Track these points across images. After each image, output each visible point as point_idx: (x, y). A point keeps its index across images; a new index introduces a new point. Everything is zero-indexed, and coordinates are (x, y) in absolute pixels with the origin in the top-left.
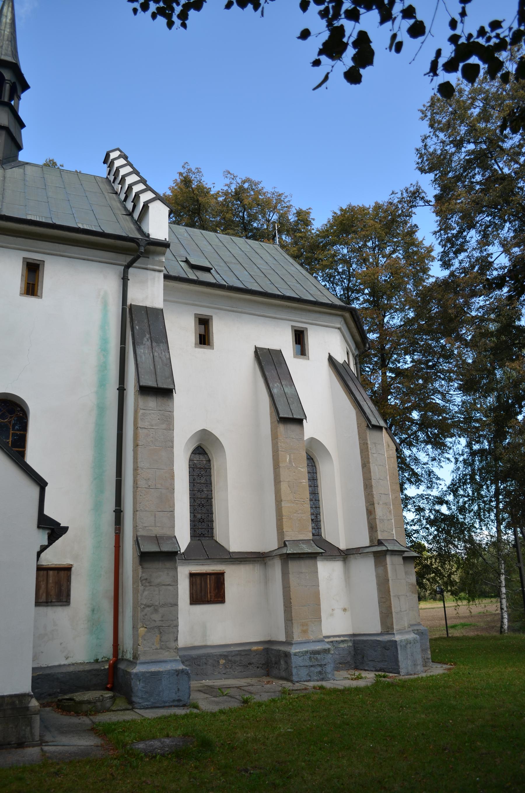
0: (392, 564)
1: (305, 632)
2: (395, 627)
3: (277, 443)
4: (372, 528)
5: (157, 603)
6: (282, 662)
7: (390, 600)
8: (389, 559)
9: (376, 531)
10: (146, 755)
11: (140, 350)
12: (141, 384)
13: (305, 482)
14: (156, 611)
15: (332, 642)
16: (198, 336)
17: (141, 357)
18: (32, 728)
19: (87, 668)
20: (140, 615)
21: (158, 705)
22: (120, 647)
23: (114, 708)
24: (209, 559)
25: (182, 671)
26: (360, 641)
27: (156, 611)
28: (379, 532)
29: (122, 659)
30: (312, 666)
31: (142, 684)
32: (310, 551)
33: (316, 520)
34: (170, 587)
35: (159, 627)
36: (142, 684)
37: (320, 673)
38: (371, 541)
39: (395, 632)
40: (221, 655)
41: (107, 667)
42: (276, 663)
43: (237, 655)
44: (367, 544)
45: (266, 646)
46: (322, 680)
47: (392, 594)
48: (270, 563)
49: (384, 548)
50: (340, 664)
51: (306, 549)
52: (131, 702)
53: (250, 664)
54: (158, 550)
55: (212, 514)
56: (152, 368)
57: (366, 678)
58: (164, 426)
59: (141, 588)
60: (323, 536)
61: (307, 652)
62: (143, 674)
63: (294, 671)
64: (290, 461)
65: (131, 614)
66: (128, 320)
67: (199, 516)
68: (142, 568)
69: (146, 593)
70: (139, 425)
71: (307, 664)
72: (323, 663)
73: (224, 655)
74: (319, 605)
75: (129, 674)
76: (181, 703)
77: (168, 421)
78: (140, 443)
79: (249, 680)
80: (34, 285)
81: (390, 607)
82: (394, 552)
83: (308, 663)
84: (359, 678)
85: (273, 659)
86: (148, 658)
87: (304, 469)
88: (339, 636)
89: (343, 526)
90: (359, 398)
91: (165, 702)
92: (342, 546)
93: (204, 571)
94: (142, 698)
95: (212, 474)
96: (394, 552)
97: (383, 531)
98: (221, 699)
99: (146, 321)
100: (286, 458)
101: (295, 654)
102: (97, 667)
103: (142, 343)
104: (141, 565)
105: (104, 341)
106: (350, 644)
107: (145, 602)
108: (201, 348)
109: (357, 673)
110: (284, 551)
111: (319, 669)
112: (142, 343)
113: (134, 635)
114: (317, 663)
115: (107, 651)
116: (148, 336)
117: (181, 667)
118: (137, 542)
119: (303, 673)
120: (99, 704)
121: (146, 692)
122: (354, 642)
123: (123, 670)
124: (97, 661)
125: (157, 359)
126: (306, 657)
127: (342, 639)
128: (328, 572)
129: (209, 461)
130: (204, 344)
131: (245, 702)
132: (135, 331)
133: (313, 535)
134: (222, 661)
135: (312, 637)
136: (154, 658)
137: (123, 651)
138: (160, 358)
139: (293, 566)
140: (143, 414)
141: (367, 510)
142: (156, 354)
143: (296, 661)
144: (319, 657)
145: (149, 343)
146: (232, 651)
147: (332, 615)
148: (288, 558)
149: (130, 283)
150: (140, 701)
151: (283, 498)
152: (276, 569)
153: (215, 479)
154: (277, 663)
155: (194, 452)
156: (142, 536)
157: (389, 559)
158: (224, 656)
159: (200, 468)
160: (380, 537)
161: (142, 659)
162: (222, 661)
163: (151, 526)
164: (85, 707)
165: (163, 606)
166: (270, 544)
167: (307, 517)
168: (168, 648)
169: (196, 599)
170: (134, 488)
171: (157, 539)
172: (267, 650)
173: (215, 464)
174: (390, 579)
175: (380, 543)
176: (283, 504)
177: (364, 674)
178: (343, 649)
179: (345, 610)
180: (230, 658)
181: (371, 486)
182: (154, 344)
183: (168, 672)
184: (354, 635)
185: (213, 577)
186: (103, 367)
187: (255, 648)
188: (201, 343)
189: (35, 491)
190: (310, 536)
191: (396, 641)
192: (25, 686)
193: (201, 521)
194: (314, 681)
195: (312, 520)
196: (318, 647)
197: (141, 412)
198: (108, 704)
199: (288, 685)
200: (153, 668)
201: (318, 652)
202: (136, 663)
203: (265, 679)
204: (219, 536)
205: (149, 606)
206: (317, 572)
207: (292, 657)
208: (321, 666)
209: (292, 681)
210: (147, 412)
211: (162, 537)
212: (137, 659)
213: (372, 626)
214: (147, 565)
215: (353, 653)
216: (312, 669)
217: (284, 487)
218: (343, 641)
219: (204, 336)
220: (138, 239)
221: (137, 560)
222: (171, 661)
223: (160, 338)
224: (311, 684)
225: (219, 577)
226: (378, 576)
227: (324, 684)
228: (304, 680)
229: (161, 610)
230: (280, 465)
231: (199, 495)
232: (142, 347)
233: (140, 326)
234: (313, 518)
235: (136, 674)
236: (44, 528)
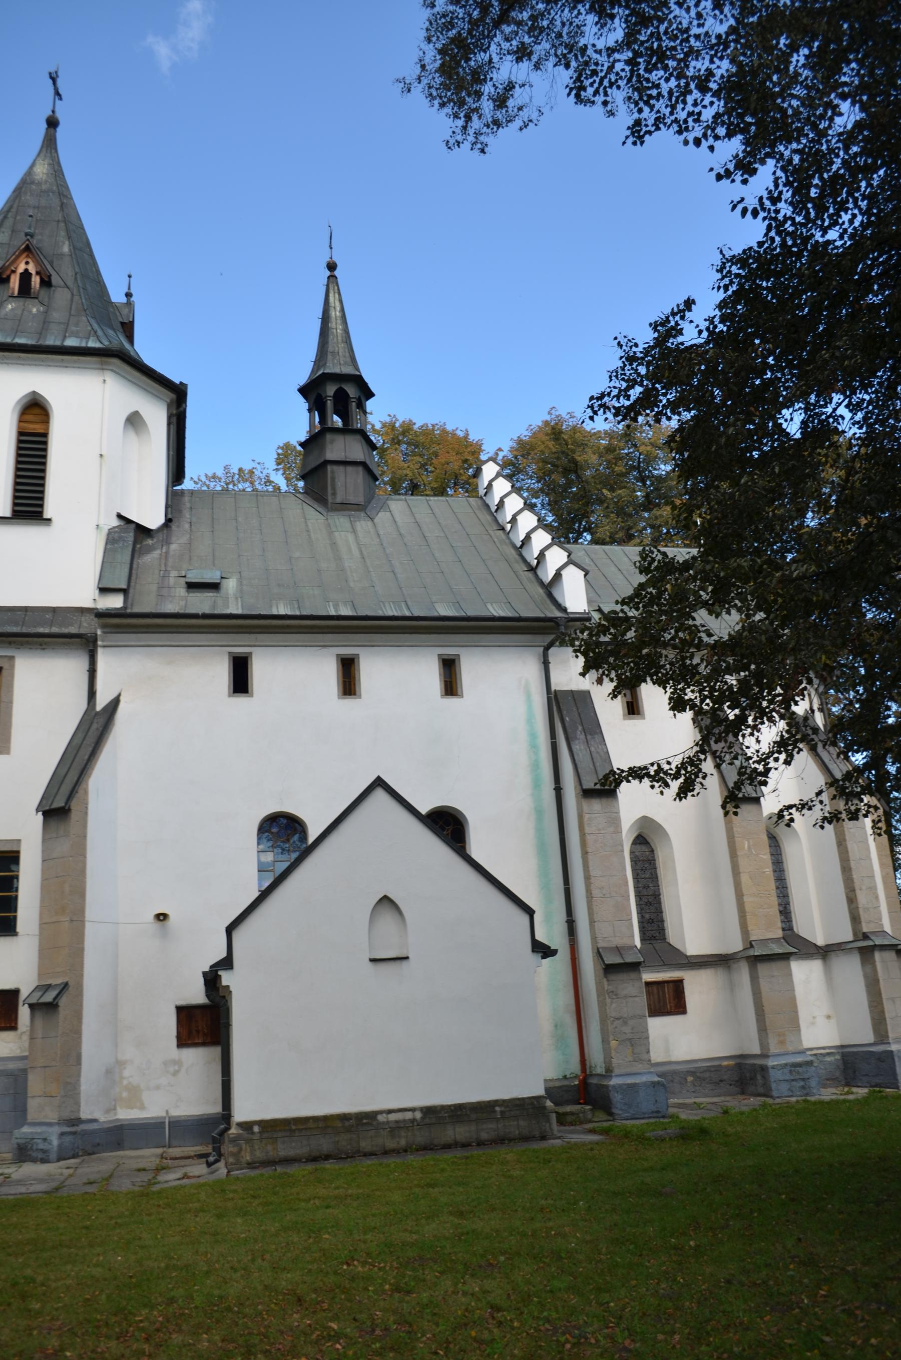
0: (883, 961)
1: (782, 1042)
2: (890, 1035)
3: (732, 828)
4: (855, 919)
5: (625, 1016)
6: (759, 1077)
7: (882, 1004)
8: (877, 955)
9: (860, 922)
10: (656, 1139)
11: (577, 747)
12: (584, 787)
13: (769, 870)
14: (625, 1023)
15: (815, 1055)
16: (625, 705)
17: (578, 755)
18: (550, 1125)
19: (557, 1084)
20: (610, 1028)
21: (637, 1116)
22: (588, 1063)
23: (595, 1119)
24: (666, 965)
25: (658, 1082)
26: (849, 1052)
27: (625, 1023)
28: (864, 924)
29: (591, 1075)
30: (793, 1080)
31: (620, 1096)
32: (781, 951)
33: (785, 912)
34: (637, 999)
35: (630, 1040)
36: (620, 1096)
37: (803, 1087)
38: (855, 934)
39: (891, 1040)
40: (688, 1072)
41: (577, 1083)
42: (751, 1079)
43: (705, 1071)
44: (851, 938)
45: (738, 1061)
46: (807, 1095)
47: (884, 996)
48: (735, 966)
49: (871, 943)
50: (828, 1080)
51: (777, 949)
52: (611, 1114)
53: (721, 1081)
54: (622, 961)
55: (662, 912)
56: (591, 766)
57: (857, 1093)
58: (611, 829)
59: (608, 1000)
60: (795, 930)
61: (786, 1065)
62: (620, 1086)
63: (774, 1086)
64: (749, 848)
65: (598, 1028)
66: (555, 708)
67: (647, 916)
68: (608, 980)
69: (614, 1005)
70: (586, 831)
71: (788, 1078)
72: (806, 1076)
73: (692, 1072)
74: (796, 1012)
75: (607, 1086)
76: (660, 1115)
77: (615, 821)
78: (589, 850)
79: (722, 1098)
80: (451, 682)
81: (883, 1012)
82: (883, 947)
83: (788, 1077)
84: (848, 1093)
85: (748, 1075)
86: (623, 1071)
87: (766, 856)
88: (824, 1048)
89: (818, 919)
90: (826, 761)
91: (644, 1113)
92: (820, 942)
93: (660, 979)
94: (621, 1110)
95: (657, 866)
96: (883, 947)
97: (870, 922)
98: (699, 1112)
99: (575, 709)
100: (744, 845)
101: (773, 1067)
102: (566, 1083)
103: (576, 738)
104: (606, 977)
105: (533, 736)
106: (838, 1057)
107: (613, 1014)
108: (630, 719)
109: (846, 1089)
110: (752, 952)
111: (802, 1083)
112: (576, 738)
113: (604, 1050)
114: (798, 1077)
115: (574, 1067)
116: (580, 728)
117: (657, 1079)
118: (598, 954)
119: (784, 1088)
120: (581, 1115)
121: (625, 1104)
122: (843, 1055)
123: (596, 1085)
124: (565, 1077)
125: (594, 755)
126: (786, 1070)
127: (828, 1051)
128: (805, 974)
129: (652, 851)
130: (633, 714)
131: (726, 1112)
132: (567, 724)
133: (783, 929)
134: (690, 1079)
135: (791, 1049)
136: (629, 1070)
137: (591, 1067)
138: (598, 753)
139: (763, 969)
140: (589, 819)
141: (847, 897)
142: (593, 749)
143: (774, 1075)
144: (800, 1069)
145: (582, 737)
146: (699, 1068)
147: (813, 1024)
148: (755, 961)
149: (552, 667)
150: (620, 1112)
151: (745, 891)
152: (743, 973)
153: (662, 872)
154: (753, 1078)
155: (634, 843)
156: (603, 948)
157: (877, 955)
158: (692, 1073)
159: (643, 861)
160: (865, 930)
161: (617, 1071)
162: (690, 1079)
163: (609, 936)
164: (569, 1118)
165: (633, 1017)
166: (735, 945)
167: (775, 910)
168: (640, 1061)
169: (657, 1010)
170: (587, 897)
171: (618, 950)
172: (739, 1066)
173: (660, 853)
174: (881, 979)
175: (866, 936)
176: (746, 899)
177: (854, 1090)
178: (830, 1063)
179: (829, 1017)
180: (698, 1074)
181: (850, 869)
182: (589, 737)
183: (645, 1084)
184: (842, 1047)
185: (671, 985)
186: (535, 766)
187: (725, 1063)
188: (629, 714)
189: (526, 919)
190: (779, 934)
191: (892, 1052)
192: (540, 1091)
193: (651, 921)
194: (796, 1096)
195: (781, 912)
196: (799, 1059)
197: (586, 817)
198: (589, 1116)
199: (769, 1101)
200: (630, 1080)
201: (799, 1065)
202: (611, 1077)
203: (740, 1097)
204: (672, 938)
205: (618, 1019)
206: (791, 975)
207: (771, 1071)
208: (803, 1080)
209: (772, 1097)
210: (593, 816)
211: (623, 948)
212: (611, 1071)
213: (862, 1034)
214: (612, 977)
215: (842, 1067)
216: (794, 1083)
217: (745, 879)
218: (828, 1054)
219: (632, 703)
220: (556, 618)
221: (601, 972)
222: (645, 1073)
223: (593, 728)
224: (794, 1099)
225: (678, 986)
226: (866, 976)
227: (808, 1098)
228: (783, 1092)
229: (631, 1022)
230: (738, 853)
231: (645, 892)
232: (577, 742)
233: (568, 715)
234: (782, 909)
235: (614, 1086)
236: (537, 952)
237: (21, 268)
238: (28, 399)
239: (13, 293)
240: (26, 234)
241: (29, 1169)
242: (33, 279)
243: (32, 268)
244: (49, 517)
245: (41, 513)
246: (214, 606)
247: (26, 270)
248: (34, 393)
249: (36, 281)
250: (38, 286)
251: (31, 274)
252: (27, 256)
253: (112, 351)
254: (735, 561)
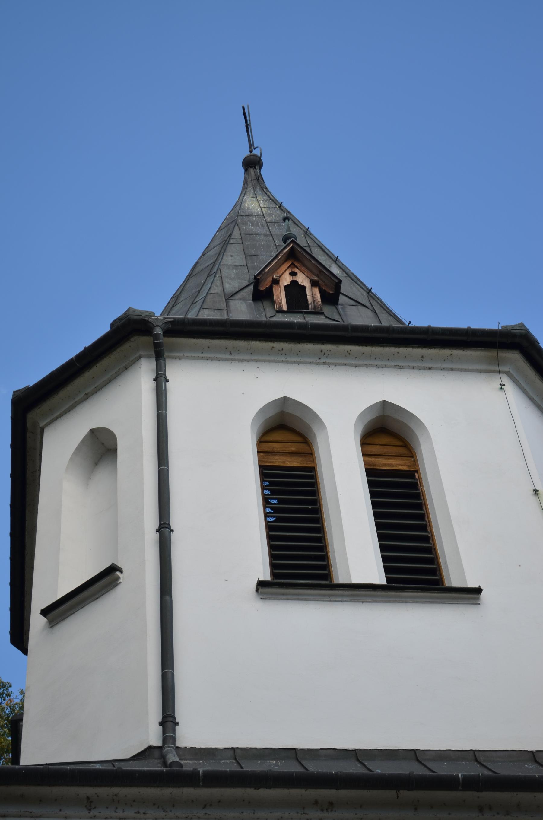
237: (286, 280)
238: (271, 413)
239: (281, 307)
240: (500, 385)
241: (30, 811)
242: (308, 293)
243: (302, 279)
244: (472, 584)
245: (328, 576)
246: (330, 267)
247: (294, 283)
248: (384, 403)
249: (313, 295)
250: (320, 302)
251: (304, 288)
252: (293, 265)
254: (217, 286)
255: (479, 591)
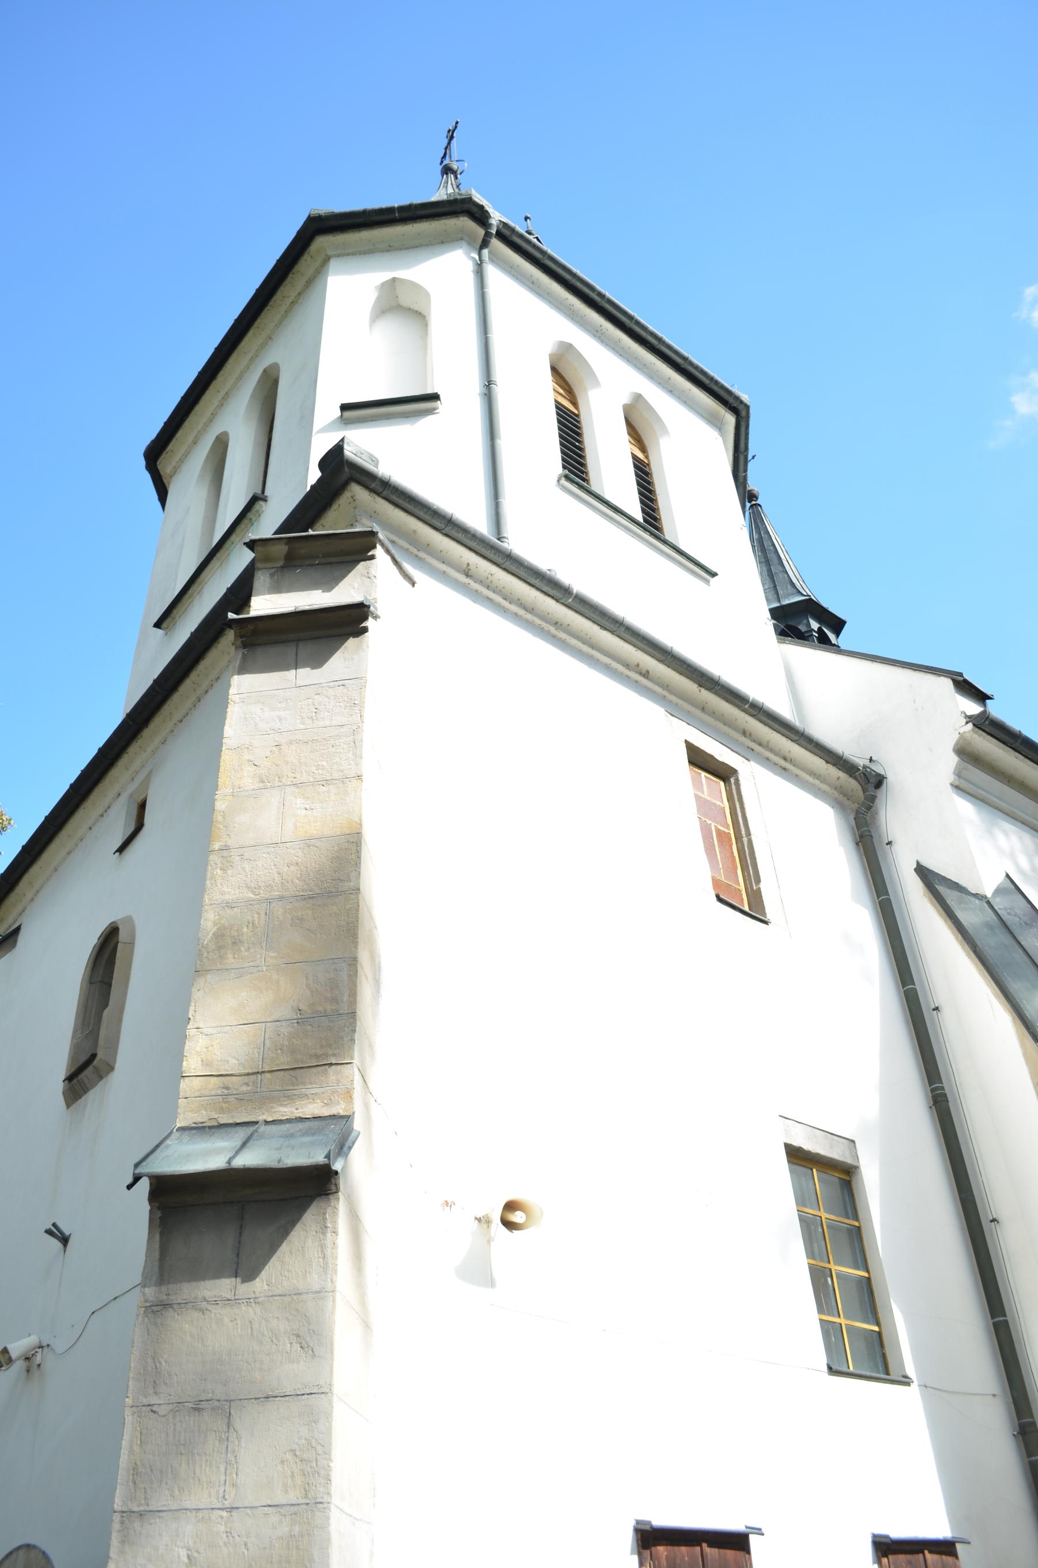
253: (742, 402)
255: (713, 575)
